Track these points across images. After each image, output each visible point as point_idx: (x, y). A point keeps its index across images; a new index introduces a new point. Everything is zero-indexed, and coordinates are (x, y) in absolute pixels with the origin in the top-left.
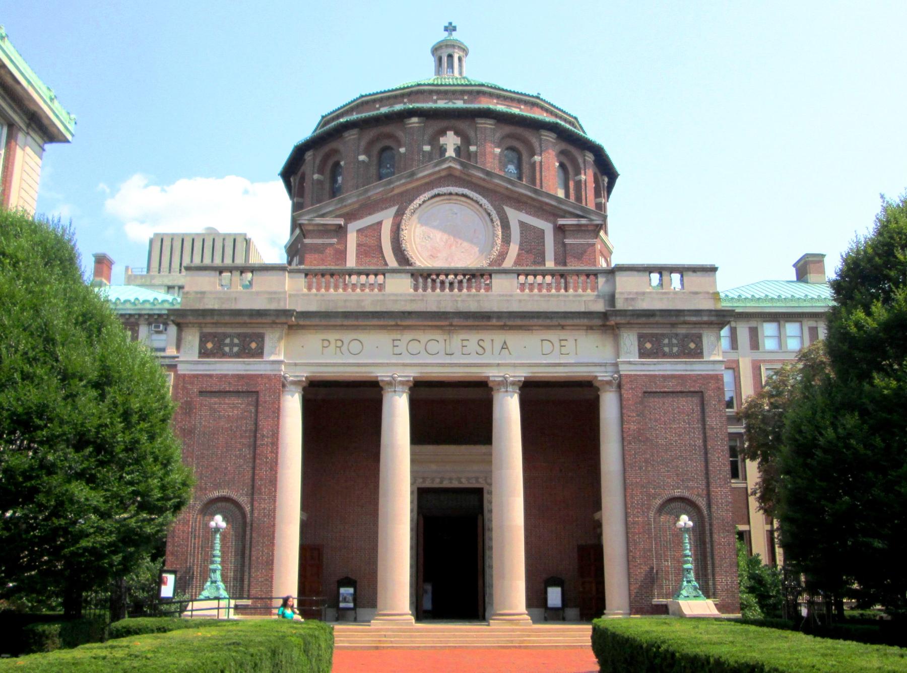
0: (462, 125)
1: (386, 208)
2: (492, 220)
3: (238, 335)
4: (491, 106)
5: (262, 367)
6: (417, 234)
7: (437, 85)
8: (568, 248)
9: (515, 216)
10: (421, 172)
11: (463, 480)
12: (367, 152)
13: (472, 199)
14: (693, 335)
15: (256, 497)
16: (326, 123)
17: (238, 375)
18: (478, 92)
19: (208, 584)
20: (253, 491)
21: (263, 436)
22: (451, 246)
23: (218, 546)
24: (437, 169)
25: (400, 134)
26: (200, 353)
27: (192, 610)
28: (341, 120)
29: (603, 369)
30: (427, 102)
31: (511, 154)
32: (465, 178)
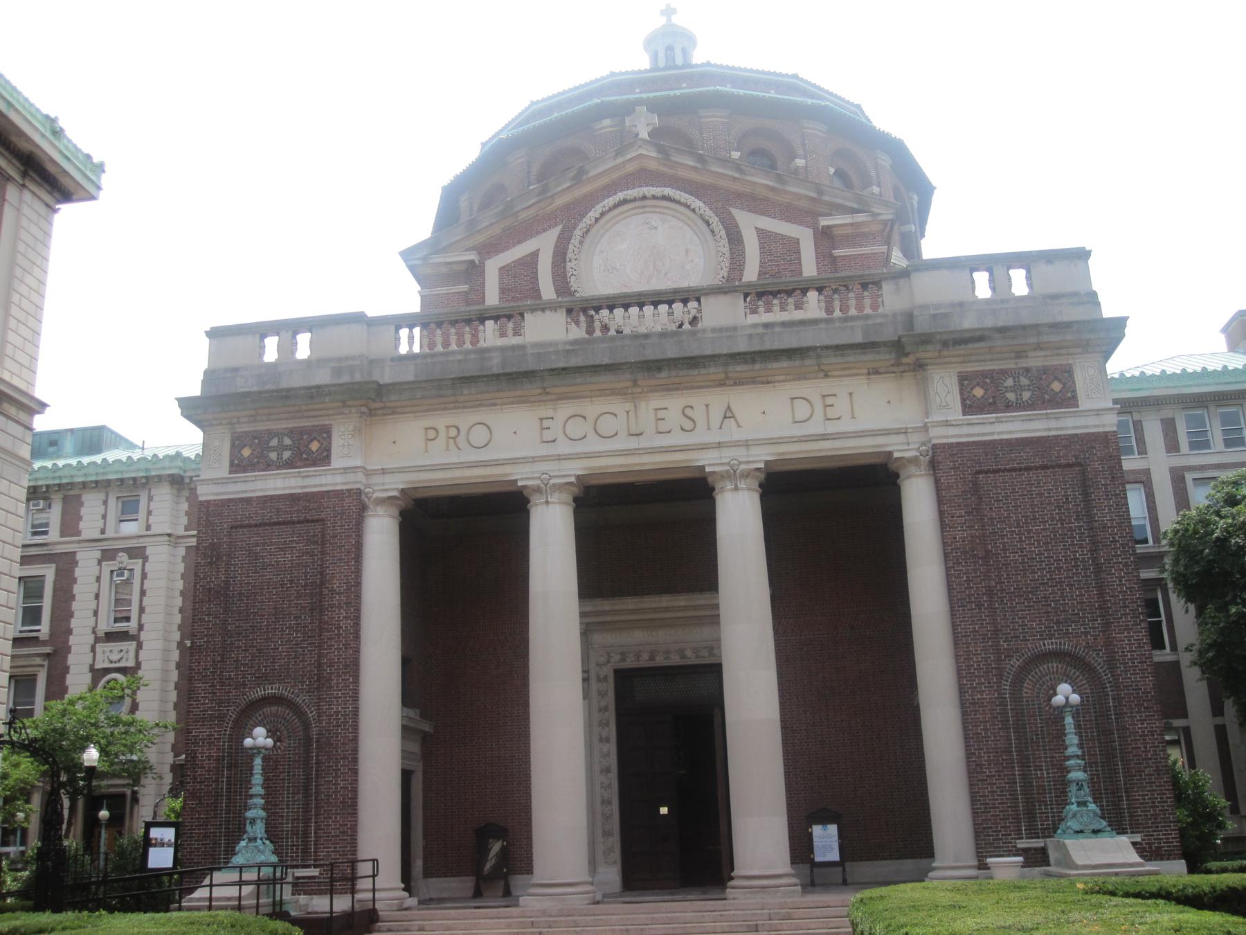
1: (545, 230)
2: (713, 232)
3: (291, 432)
9: (749, 224)
11: (689, 653)
13: (679, 202)
17: (291, 495)
19: (243, 843)
20: (320, 683)
21: (333, 591)
23: (257, 779)
24: (620, 160)
26: (232, 465)
27: (241, 883)
29: (901, 438)
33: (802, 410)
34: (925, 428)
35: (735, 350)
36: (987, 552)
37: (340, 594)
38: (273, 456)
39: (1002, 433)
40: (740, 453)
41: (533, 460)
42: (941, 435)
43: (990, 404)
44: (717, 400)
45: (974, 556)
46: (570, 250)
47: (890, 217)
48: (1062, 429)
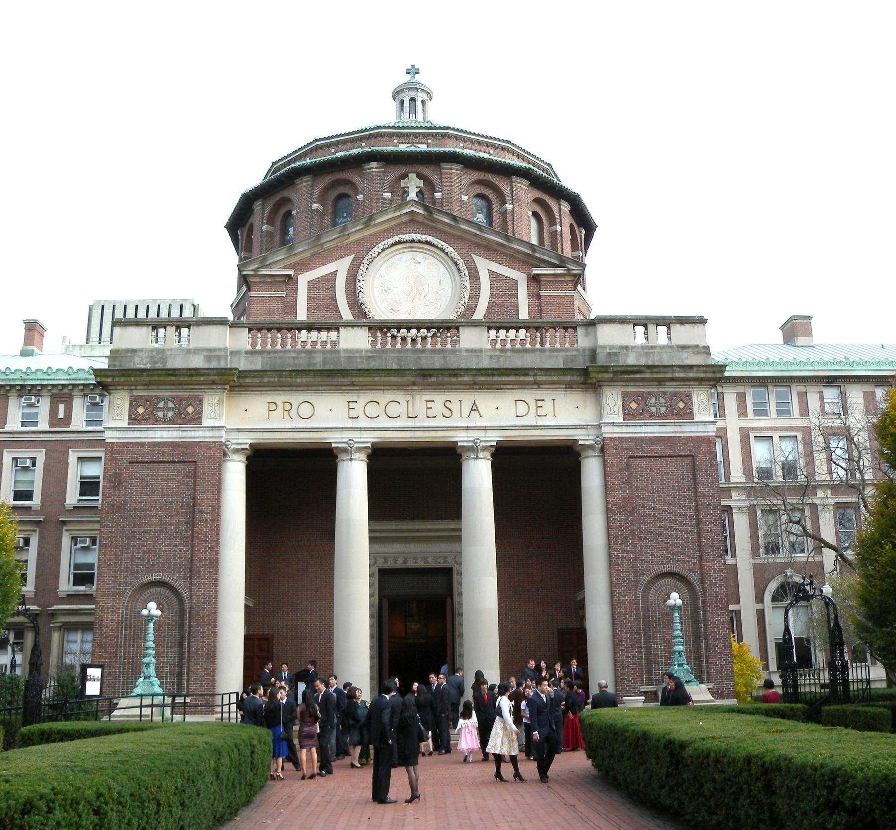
0: (427, 171)
2: (459, 270)
4: (457, 150)
5: (200, 433)
6: (375, 285)
7: (399, 128)
8: (544, 300)
9: (485, 266)
10: (380, 217)
11: (430, 560)
12: (321, 200)
13: (437, 247)
14: (681, 393)
15: (195, 581)
16: (279, 169)
17: (173, 442)
18: (443, 134)
19: (141, 679)
20: (191, 573)
21: (202, 511)
23: (151, 637)
24: (398, 213)
25: (357, 180)
26: (130, 418)
28: (293, 165)
29: (584, 432)
30: (387, 146)
31: (481, 203)
32: (431, 223)
33: (522, 408)
34: (599, 427)
35: (480, 366)
36: (634, 508)
37: (207, 513)
38: (160, 414)
40: (480, 435)
41: (343, 429)
44: (468, 398)
45: (625, 510)
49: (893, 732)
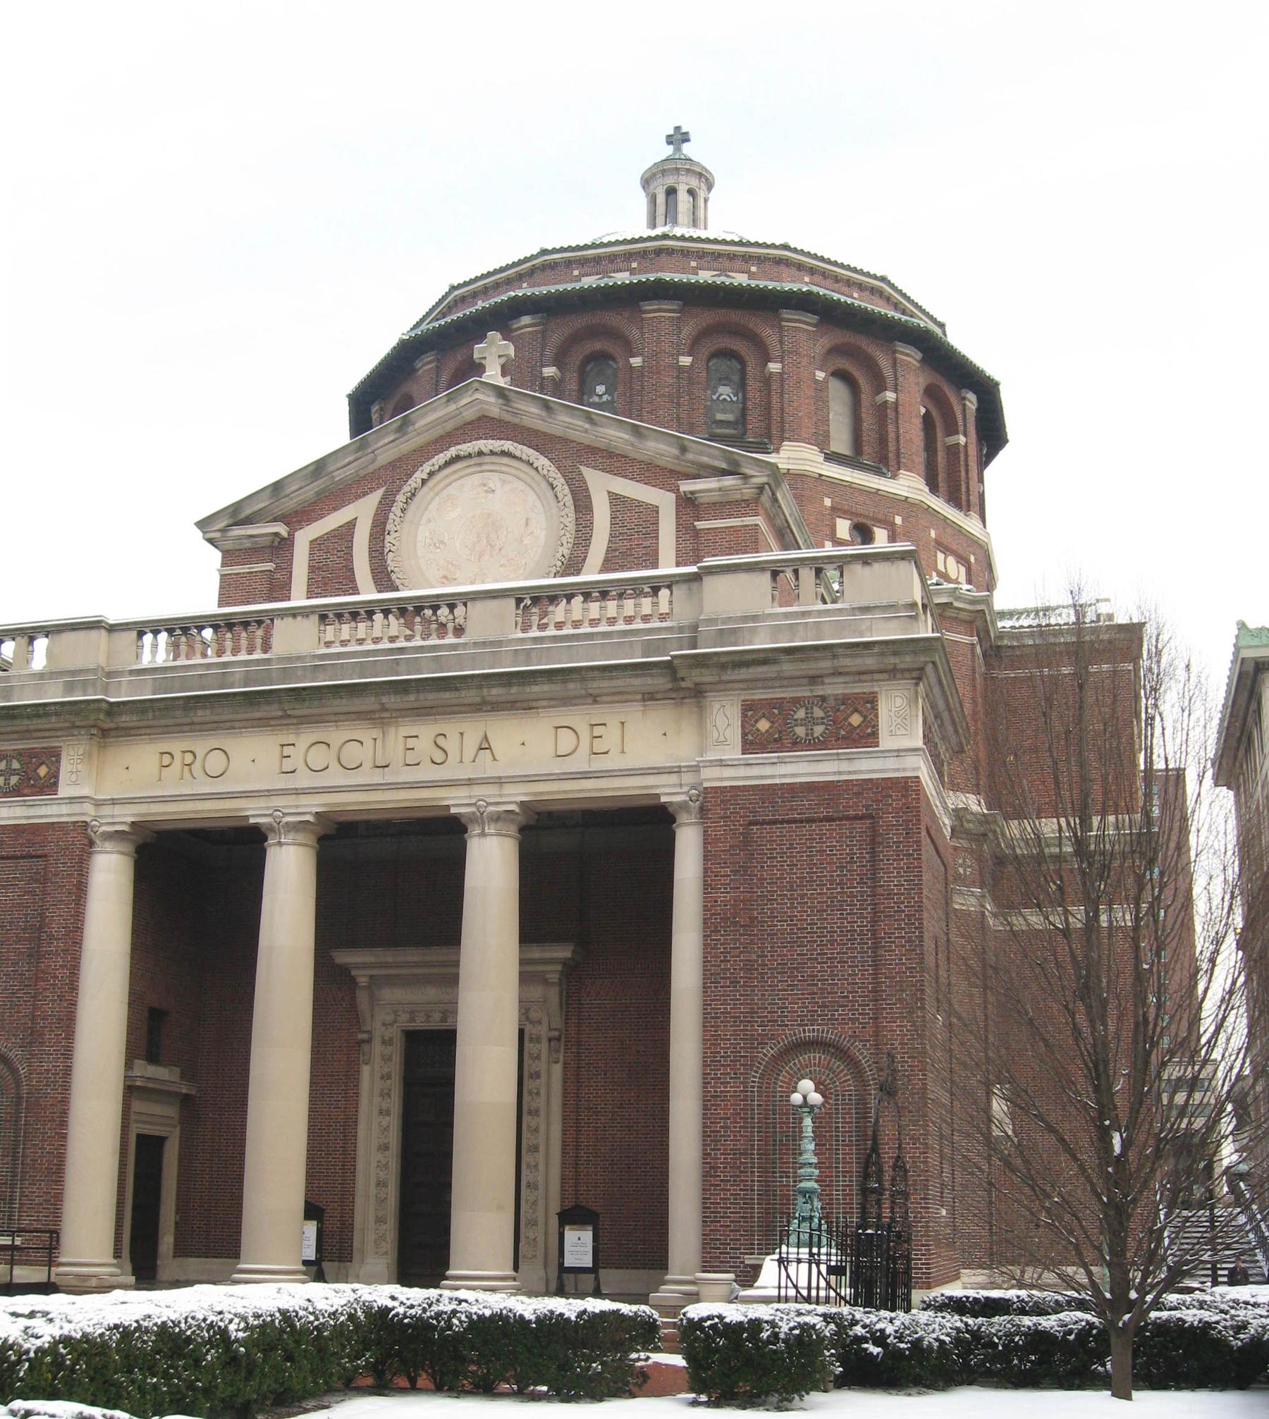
1: (365, 494)
3: (20, 754)
21: (51, 937)
22: (481, 554)
25: (634, 333)
29: (673, 779)
31: (722, 365)
36: (752, 919)
39: (785, 776)
41: (270, 793)
42: (714, 777)
43: (775, 740)
45: (735, 924)
46: (390, 521)
47: (764, 480)
48: (855, 772)
49: (7, 1346)
